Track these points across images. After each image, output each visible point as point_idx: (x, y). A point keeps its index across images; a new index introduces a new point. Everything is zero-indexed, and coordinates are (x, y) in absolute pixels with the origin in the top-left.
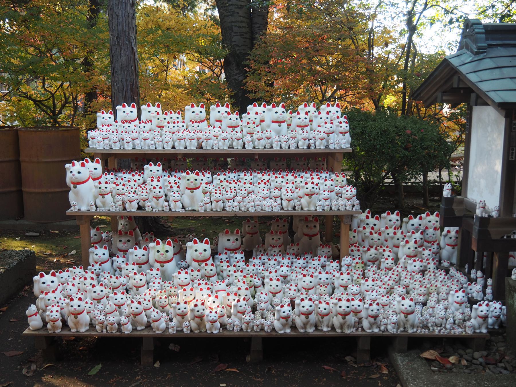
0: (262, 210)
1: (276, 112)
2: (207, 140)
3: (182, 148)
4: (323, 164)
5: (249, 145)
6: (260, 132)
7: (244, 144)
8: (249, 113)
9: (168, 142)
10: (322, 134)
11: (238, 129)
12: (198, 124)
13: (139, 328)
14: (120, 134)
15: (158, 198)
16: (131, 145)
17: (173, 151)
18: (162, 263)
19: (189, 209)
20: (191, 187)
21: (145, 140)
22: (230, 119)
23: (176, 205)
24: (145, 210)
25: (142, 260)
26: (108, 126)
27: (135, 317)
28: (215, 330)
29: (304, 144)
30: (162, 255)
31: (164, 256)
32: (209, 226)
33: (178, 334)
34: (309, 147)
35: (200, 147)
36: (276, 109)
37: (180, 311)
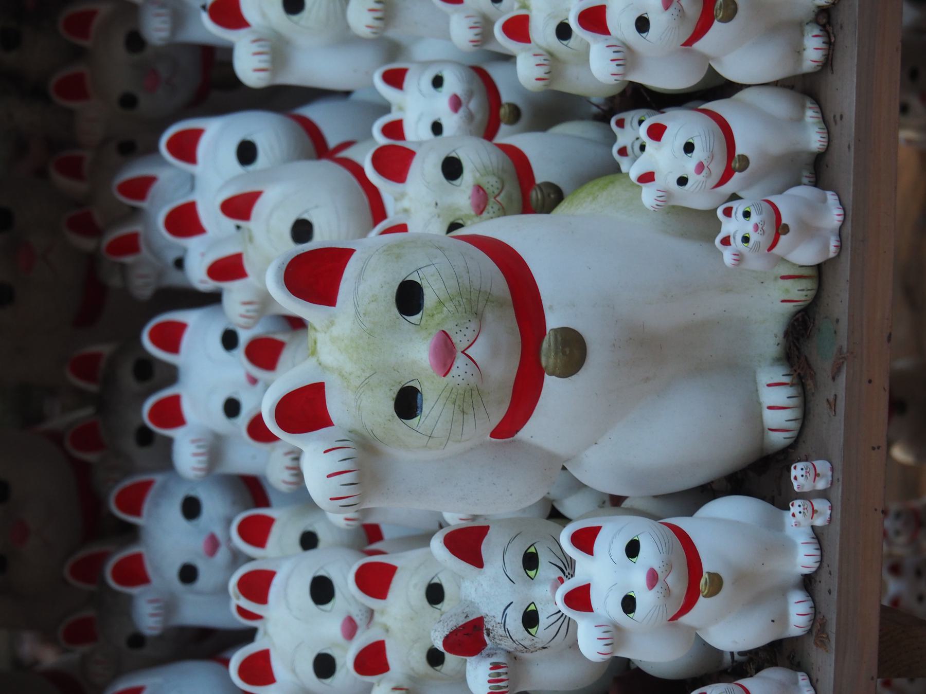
19: (776, 405)
20: (503, 370)
23: (743, 578)
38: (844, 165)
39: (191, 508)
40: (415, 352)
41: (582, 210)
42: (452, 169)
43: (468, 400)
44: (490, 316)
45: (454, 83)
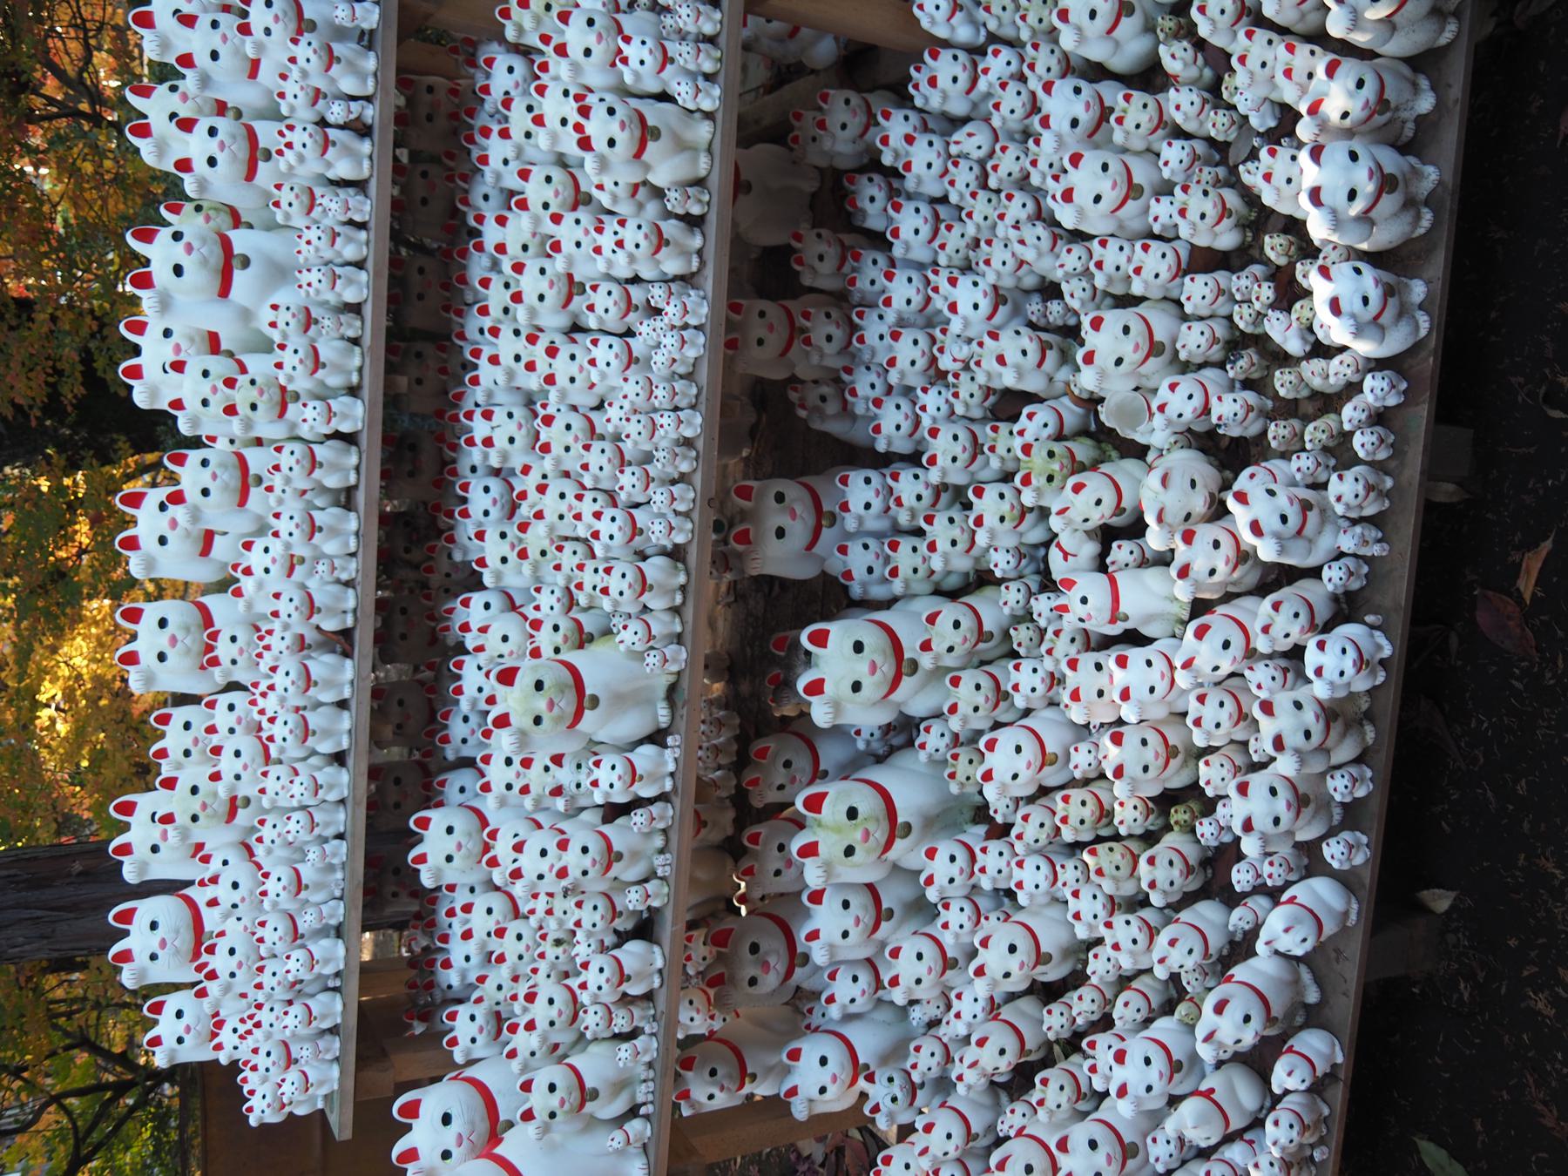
0: (689, 377)
1: (178, 270)
2: (312, 608)
3: (346, 721)
4: (430, 89)
5: (345, 417)
6: (278, 355)
7: (337, 435)
8: (177, 404)
9: (317, 787)
10: (302, 51)
11: (258, 460)
12: (223, 639)
14: (269, 997)
15: (612, 856)
16: (320, 947)
19: (663, 716)
20: (571, 709)
21: (300, 886)
22: (205, 492)
23: (650, 775)
24: (657, 910)
25: (866, 908)
26: (219, 1024)
29: (349, 152)
34: (361, 130)
35: (342, 642)
36: (160, 271)
38: (688, 638)
39: (466, 719)
40: (540, 704)
41: (598, 649)
42: (556, 628)
43: (558, 720)
45: (558, 593)
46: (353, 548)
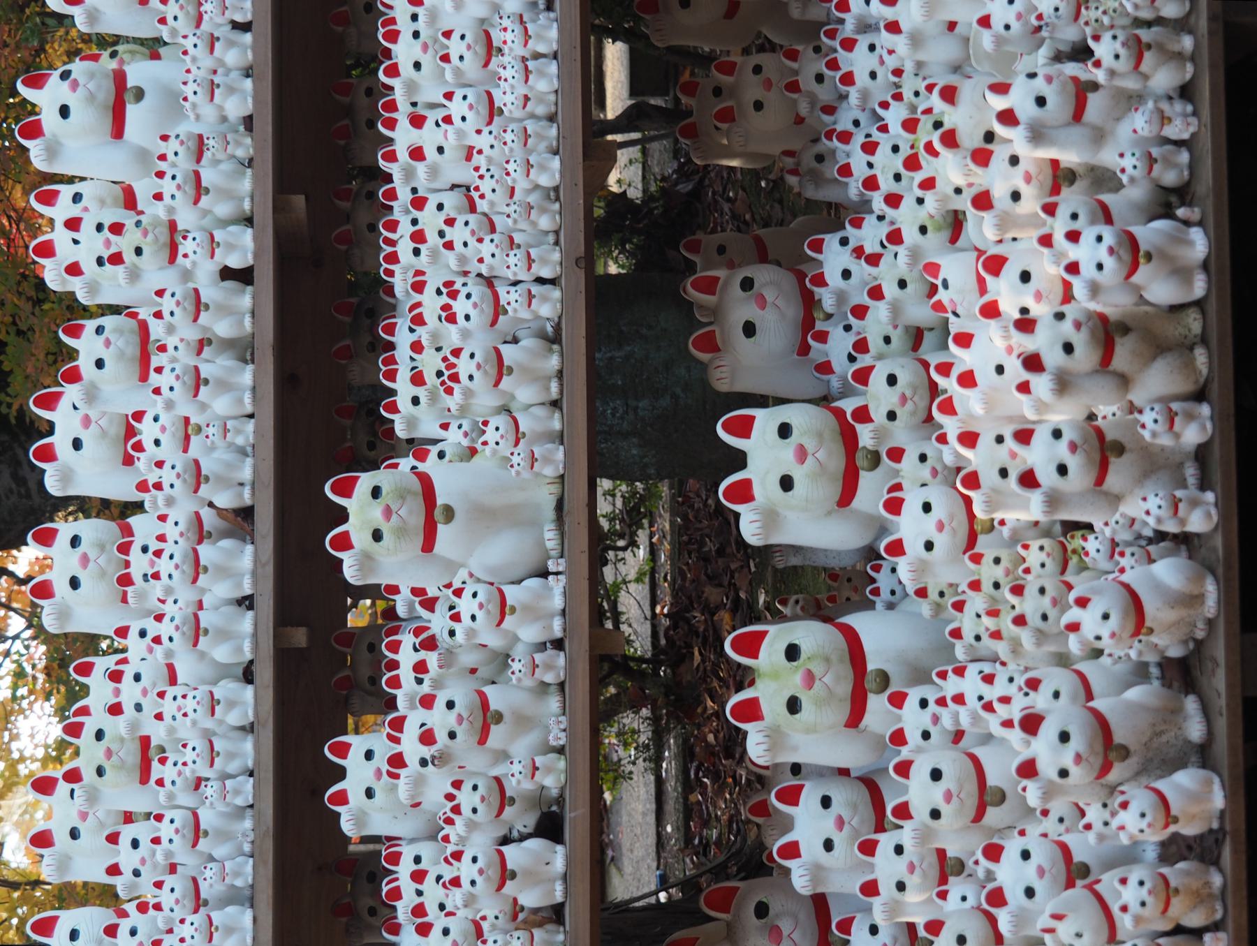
2: (198, 477)
3: (246, 622)
5: (231, 247)
13: (1195, 730)
15: (486, 718)
17: (265, 673)
18: (862, 683)
19: (550, 537)
20: (419, 520)
21: (197, 832)
25: (854, 807)
27: (1124, 752)
28: (1190, 243)
30: (810, 679)
31: (817, 669)
32: (648, 413)
33: (1217, 476)
37: (1073, 462)
44: (409, 498)
46: (249, 409)
